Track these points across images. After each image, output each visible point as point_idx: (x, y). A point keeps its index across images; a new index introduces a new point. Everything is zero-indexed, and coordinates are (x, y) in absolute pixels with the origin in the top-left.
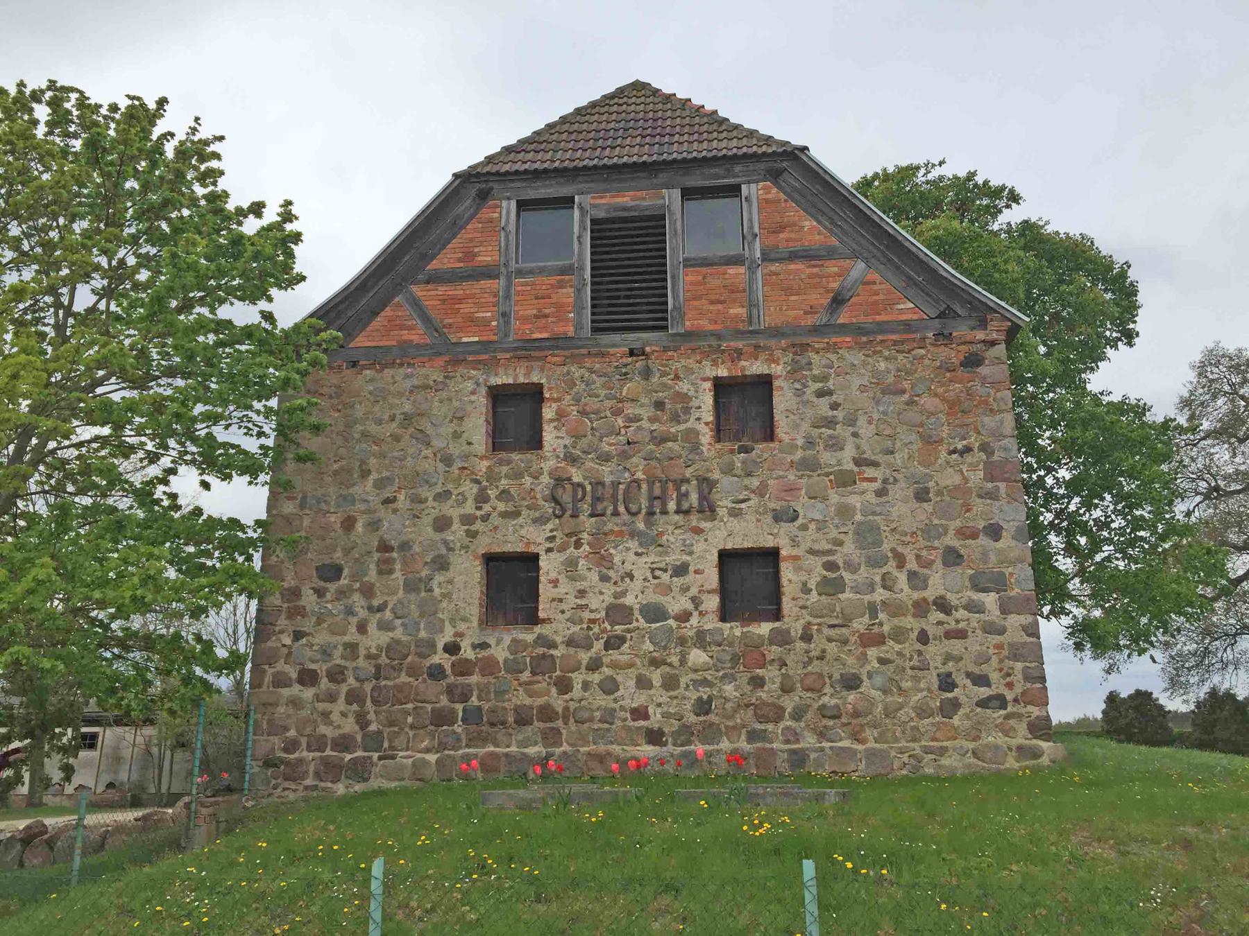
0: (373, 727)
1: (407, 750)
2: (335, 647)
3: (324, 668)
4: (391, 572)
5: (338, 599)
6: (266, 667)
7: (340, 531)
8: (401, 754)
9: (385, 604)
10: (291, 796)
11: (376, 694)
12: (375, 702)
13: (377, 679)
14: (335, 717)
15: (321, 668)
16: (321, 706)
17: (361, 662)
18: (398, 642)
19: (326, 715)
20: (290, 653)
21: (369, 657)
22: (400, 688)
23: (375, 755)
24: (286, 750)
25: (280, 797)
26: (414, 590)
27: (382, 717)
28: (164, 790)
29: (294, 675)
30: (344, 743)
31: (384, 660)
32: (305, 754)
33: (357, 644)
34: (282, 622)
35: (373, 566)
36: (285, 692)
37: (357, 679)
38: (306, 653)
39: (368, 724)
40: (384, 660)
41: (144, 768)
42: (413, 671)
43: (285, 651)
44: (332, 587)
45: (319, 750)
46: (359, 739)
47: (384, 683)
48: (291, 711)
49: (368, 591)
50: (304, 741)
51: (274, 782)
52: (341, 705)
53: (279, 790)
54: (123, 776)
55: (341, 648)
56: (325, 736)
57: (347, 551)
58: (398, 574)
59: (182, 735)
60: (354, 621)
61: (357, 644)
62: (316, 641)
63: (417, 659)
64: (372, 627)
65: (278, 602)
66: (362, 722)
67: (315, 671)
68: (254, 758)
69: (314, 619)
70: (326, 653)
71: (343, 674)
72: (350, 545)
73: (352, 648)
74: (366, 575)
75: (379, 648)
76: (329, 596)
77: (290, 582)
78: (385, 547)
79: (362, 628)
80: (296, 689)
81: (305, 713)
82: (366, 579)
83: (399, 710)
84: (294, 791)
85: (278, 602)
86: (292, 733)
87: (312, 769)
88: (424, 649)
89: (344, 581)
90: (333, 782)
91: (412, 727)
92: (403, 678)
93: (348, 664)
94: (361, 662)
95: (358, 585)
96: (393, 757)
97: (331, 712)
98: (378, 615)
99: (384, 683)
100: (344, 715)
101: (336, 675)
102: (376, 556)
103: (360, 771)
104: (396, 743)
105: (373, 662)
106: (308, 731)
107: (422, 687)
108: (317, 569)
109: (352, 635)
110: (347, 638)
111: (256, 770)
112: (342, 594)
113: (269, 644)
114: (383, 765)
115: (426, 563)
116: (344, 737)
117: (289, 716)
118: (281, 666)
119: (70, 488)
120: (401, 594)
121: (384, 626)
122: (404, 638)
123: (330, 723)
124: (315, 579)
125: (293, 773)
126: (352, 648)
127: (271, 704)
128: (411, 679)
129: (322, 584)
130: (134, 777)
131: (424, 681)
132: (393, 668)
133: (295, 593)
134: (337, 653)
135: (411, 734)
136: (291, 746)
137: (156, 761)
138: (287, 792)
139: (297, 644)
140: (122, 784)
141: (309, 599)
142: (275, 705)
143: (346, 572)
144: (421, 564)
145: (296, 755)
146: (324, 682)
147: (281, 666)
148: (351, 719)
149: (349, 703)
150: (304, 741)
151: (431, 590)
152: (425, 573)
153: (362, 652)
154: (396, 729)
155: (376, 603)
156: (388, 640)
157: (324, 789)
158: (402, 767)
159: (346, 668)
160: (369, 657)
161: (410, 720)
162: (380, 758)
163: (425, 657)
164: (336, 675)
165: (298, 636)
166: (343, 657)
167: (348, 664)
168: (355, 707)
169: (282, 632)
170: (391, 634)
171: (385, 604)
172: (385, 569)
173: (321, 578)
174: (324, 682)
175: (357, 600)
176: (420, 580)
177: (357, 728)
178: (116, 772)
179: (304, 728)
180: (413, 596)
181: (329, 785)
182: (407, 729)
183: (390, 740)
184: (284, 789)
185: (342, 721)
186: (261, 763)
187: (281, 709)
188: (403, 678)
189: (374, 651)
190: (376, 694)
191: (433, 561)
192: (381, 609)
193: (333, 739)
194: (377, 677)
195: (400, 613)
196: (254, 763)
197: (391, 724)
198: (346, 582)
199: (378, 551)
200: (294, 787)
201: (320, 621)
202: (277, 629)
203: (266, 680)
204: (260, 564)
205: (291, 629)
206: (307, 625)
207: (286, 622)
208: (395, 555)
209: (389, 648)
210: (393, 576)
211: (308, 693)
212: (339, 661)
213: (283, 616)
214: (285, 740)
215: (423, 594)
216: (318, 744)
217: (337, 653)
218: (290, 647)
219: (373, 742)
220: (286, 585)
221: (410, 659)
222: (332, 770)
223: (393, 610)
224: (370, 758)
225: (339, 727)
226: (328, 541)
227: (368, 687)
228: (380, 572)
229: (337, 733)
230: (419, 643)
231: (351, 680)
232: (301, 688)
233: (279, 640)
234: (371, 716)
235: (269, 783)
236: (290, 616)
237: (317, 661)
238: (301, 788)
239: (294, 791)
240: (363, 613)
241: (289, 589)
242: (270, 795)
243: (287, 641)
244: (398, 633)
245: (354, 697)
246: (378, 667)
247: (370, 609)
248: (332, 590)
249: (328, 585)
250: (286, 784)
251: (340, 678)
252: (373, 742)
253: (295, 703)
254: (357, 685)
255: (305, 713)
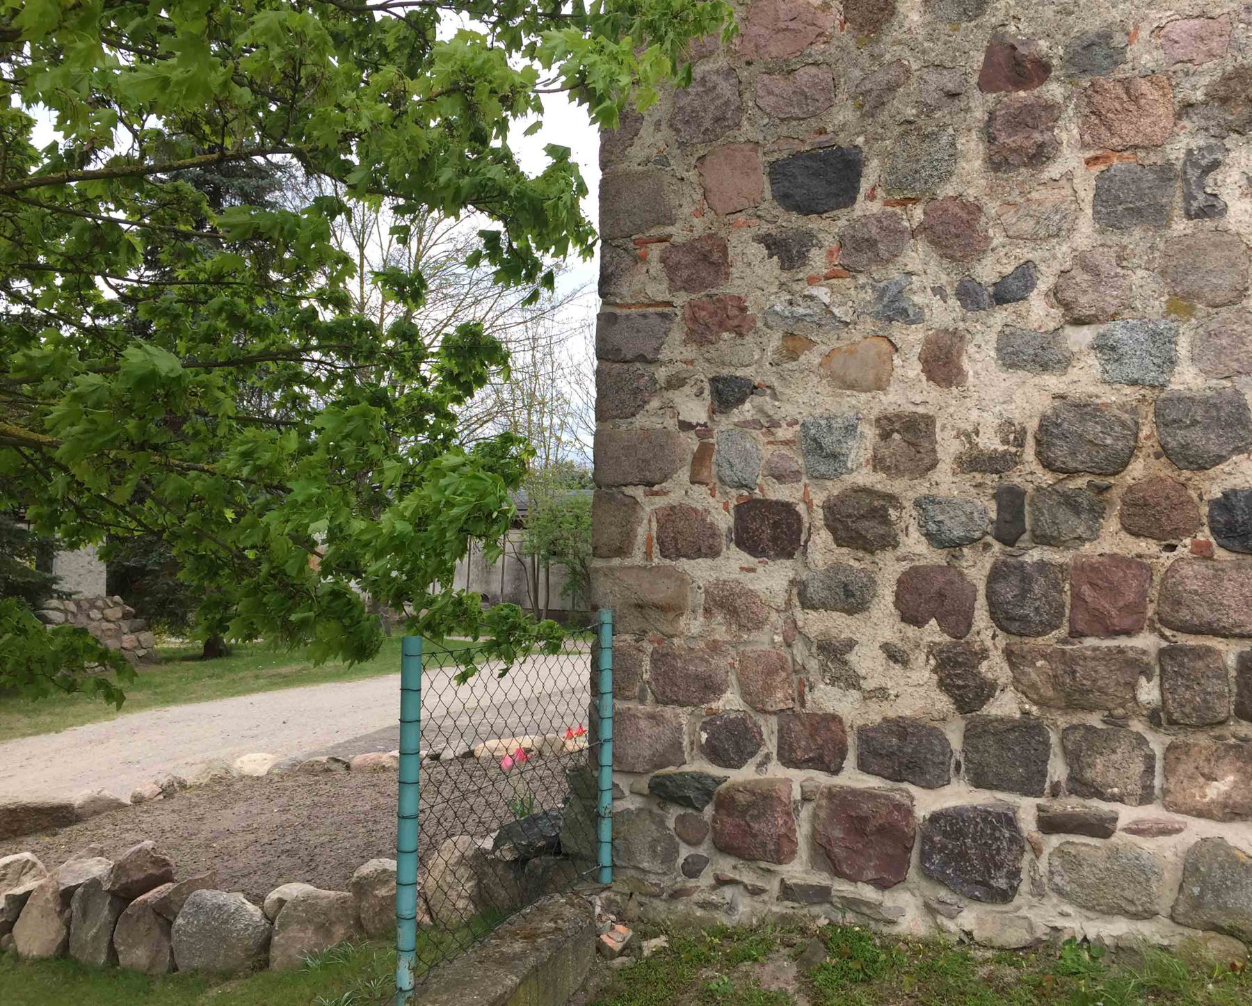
0: (1005, 705)
1: (1146, 797)
2: (850, 429)
3: (818, 498)
4: (1040, 156)
5: (849, 270)
6: (638, 492)
7: (846, 38)
8: (1127, 814)
9: (1025, 276)
10: (746, 909)
11: (1008, 591)
12: (1002, 618)
13: (1008, 540)
14: (867, 660)
15: (808, 497)
16: (816, 623)
17: (946, 481)
18: (1085, 409)
19: (834, 652)
20: (702, 456)
21: (974, 462)
22: (1096, 574)
23: (1027, 809)
24: (714, 752)
25: (704, 905)
26: (1137, 214)
27: (1038, 670)
28: (541, 605)
29: (724, 521)
30: (903, 751)
31: (1031, 474)
32: (776, 771)
33: (929, 421)
34: (676, 349)
35: (972, 150)
36: (701, 572)
37: (934, 539)
38: (755, 451)
39: (986, 690)
40: (1031, 474)
41: (518, 578)
42: (1148, 516)
43: (691, 442)
44: (828, 229)
45: (818, 763)
46: (955, 737)
47: (1035, 555)
48: (721, 632)
49: (956, 234)
50: (769, 728)
51: (685, 852)
52: (880, 623)
53: (706, 880)
54: (495, 588)
55: (869, 432)
56: (836, 719)
57: (871, 103)
58: (1070, 158)
59: (553, 543)
60: (912, 338)
61: (929, 421)
62: (788, 410)
63: (1163, 469)
64: (979, 359)
65: (659, 290)
66: (961, 679)
67: (788, 508)
68: (622, 766)
69: (774, 341)
70: (821, 449)
71: (885, 520)
72: (882, 77)
73: (910, 435)
74: (947, 176)
75: (1013, 433)
76: (818, 261)
77: (689, 224)
78: (1014, 67)
79: (942, 364)
80: (733, 563)
81: (766, 640)
82: (949, 190)
83: (1108, 656)
84: (756, 892)
85: (659, 290)
86: (730, 701)
87: (803, 830)
88: (1196, 436)
89: (866, 207)
90: (882, 885)
91: (1155, 718)
92: (1112, 540)
93: (897, 486)
94: (946, 481)
95: (918, 213)
96: (1101, 828)
97: (850, 645)
98: (1001, 316)
99: (1035, 555)
100: (894, 655)
101: (861, 523)
102: (979, 105)
103: (975, 858)
104: (1098, 769)
105: (991, 480)
106: (779, 699)
107: (1193, 576)
108: (777, 171)
109: (909, 389)
110: (893, 400)
111: (631, 803)
112: (863, 250)
113: (640, 421)
114: (1060, 852)
115: (1188, 106)
116: (901, 728)
117: (715, 647)
118: (680, 490)
119: (1149, 692)
120: (1085, 233)
121: (1022, 355)
122: (1108, 396)
123: (851, 681)
124: (770, 207)
125: (745, 830)
126: (910, 435)
127: (662, 608)
128: (1147, 547)
129: (795, 221)
130: (508, 589)
131: (1203, 553)
132: (1071, 502)
133: (709, 259)
134: (860, 449)
135: (1157, 743)
136: (732, 743)
137: (529, 570)
138: (728, 892)
139: (725, 423)
140: (495, 597)
141: (753, 274)
142: (672, 609)
143: (872, 173)
144: (1163, 112)
145: (745, 774)
146: (821, 548)
147: (680, 490)
148: (923, 673)
149: (911, 617)
150: (769, 728)
151: (1212, 209)
152: (1182, 145)
153: (948, 447)
154: (1095, 720)
155: (987, 272)
156: (1044, 404)
157: (852, 904)
158: (1141, 872)
159: (892, 499)
160: (974, 462)
161: (1149, 692)
162: (1049, 824)
163: (1202, 463)
164: (861, 523)
165: (727, 393)
166: (878, 463)
167: (897, 486)
168: (932, 632)
169: (676, 383)
170: (1053, 382)
171: (1025, 276)
172: (1019, 149)
173: (787, 200)
174: (821, 548)
175: (920, 265)
176: (1165, 173)
177: (943, 703)
178: (488, 583)
179: (769, 689)
180: (1136, 238)
181: (868, 893)
182: (1137, 726)
183: (1073, 757)
184: (721, 882)
185: (893, 679)
186: (644, 784)
187: (693, 624)
188: (1112, 540)
189: (990, 442)
190: (1008, 591)
191: (1221, 97)
192: (1003, 295)
193: (862, 731)
194: (1009, 528)
195: (1086, 303)
196: (624, 783)
197: (1075, 700)
198: (875, 207)
199: (986, 84)
200: (748, 878)
201: (794, 345)
202: (662, 374)
203: (641, 531)
204: (598, 175)
205: (703, 372)
206: (752, 357)
207: (690, 352)
208: (1054, 90)
209: (1048, 431)
210: (1053, 170)
211: (772, 580)
212: (865, 477)
213: (677, 334)
214: (712, 722)
215: (1181, 226)
216: (818, 743)
217: (860, 449)
218: (704, 431)
219: (1009, 755)
220: (678, 233)
221: (1137, 470)
222: (869, 841)
223: (1055, 295)
224: (1009, 820)
225: (881, 693)
226: (805, 75)
227: (977, 568)
228: (998, 163)
229: (875, 714)
230: (1172, 412)
231: (914, 544)
232: (746, 559)
233: (669, 407)
234: (995, 667)
235: (669, 856)
236: (700, 334)
237: (795, 476)
238: (774, 886)
239: (756, 892)
240: (944, 314)
241: (689, 247)
242: (676, 895)
243: (696, 410)
244: (1085, 378)
245: (922, 598)
246: (1010, 500)
247: (969, 295)
248: (829, 241)
249: (813, 223)
250: (725, 866)
251: (871, 528)
252: (1009, 755)
253: (731, 605)
254: (937, 557)
255: (766, 640)
